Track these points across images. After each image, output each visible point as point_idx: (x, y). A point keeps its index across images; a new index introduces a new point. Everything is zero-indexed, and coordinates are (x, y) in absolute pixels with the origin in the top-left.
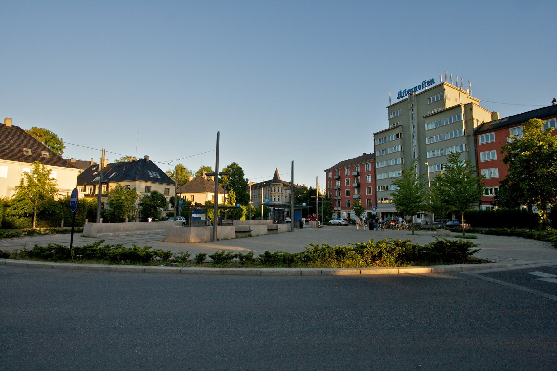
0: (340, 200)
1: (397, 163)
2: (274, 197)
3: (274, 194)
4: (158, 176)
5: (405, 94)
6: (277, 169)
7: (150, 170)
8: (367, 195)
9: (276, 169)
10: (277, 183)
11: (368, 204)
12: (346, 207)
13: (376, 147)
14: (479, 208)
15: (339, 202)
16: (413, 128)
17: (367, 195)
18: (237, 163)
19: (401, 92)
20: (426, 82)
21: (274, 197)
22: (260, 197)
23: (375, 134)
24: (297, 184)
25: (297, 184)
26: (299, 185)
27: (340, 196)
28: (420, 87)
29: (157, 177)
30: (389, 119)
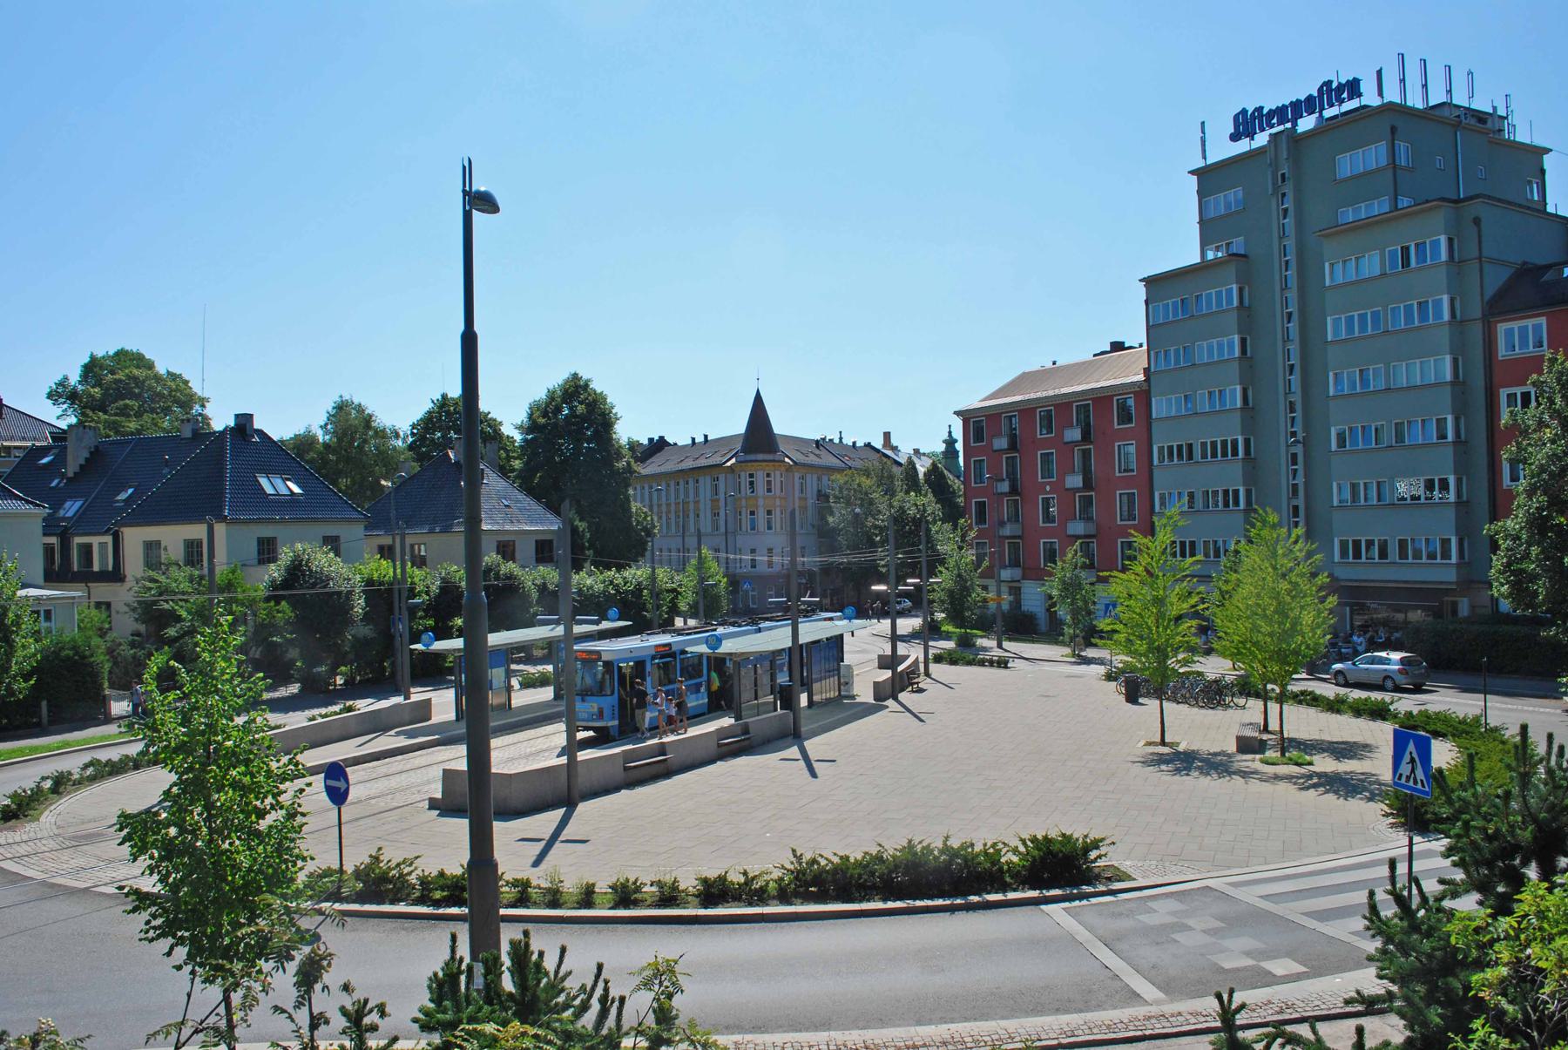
0: (1019, 537)
1: (1228, 407)
5: (1329, 99)
9: (758, 401)
10: (760, 457)
13: (1150, 331)
14: (695, 628)
16: (1286, 270)
17: (1041, 524)
18: (585, 374)
19: (1244, 111)
20: (1265, 112)
23: (1151, 282)
24: (693, 439)
25: (693, 439)
28: (1309, 105)
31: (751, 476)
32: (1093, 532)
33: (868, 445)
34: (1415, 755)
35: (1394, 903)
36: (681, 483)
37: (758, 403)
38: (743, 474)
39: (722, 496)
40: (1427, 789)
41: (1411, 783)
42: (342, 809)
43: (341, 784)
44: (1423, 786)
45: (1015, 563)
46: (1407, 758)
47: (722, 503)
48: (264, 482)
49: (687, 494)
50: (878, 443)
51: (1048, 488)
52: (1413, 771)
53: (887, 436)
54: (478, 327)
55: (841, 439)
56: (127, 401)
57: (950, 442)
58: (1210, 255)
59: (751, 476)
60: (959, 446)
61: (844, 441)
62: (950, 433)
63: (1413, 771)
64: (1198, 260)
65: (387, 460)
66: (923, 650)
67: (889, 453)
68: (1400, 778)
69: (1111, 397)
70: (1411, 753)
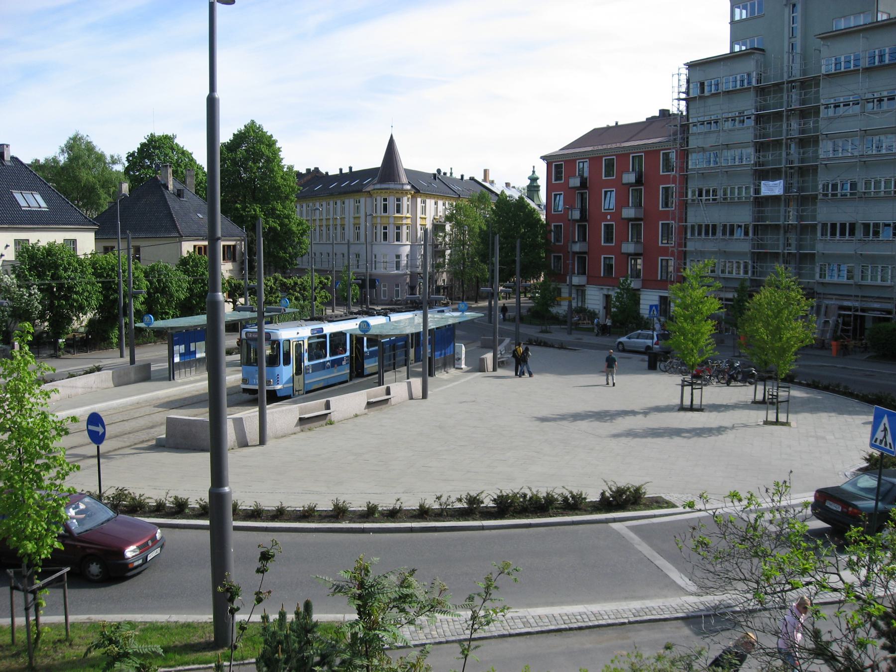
0: (585, 253)
2: (383, 231)
3: (385, 221)
4: (43, 204)
6: (395, 138)
7: (20, 188)
8: (660, 245)
9: (391, 143)
11: (661, 272)
12: (602, 275)
15: (582, 261)
17: (223, 243)
21: (385, 228)
22: (339, 228)
24: (462, 176)
25: (462, 176)
26: (466, 178)
27: (584, 240)
29: (40, 207)
30: (733, 22)
31: (385, 200)
32: (641, 251)
33: (472, 179)
34: (887, 426)
36: (331, 203)
37: (391, 145)
38: (378, 198)
39: (362, 214)
40: (893, 450)
41: (883, 445)
42: (753, 397)
43: (100, 429)
44: (891, 447)
45: (582, 272)
46: (881, 427)
47: (362, 220)
49: (335, 212)
50: (480, 178)
51: (609, 217)
52: (885, 437)
53: (486, 172)
55: (451, 174)
57: (533, 179)
58: (737, 48)
59: (385, 200)
60: (542, 183)
61: (454, 175)
62: (534, 172)
63: (885, 437)
64: (728, 51)
65: (108, 181)
67: (487, 185)
68: (876, 441)
69: (658, 151)
70: (885, 424)
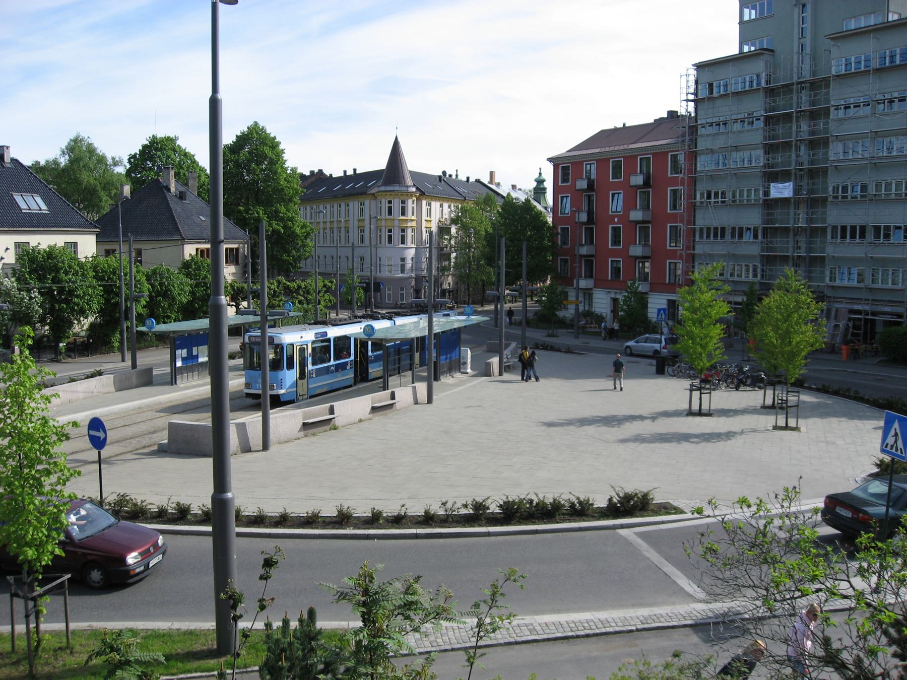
0: (592, 256)
2: (387, 234)
3: (389, 223)
4: (44, 207)
6: (399, 139)
7: (20, 191)
8: (668, 248)
9: (396, 145)
11: (670, 275)
12: (609, 278)
15: (589, 264)
21: (390, 231)
22: (343, 231)
24: (468, 178)
25: (468, 178)
26: (472, 180)
27: (592, 243)
29: (41, 210)
30: (742, 23)
31: (390, 202)
32: (649, 254)
33: (478, 181)
34: (898, 431)
35: (102, 420)
36: (335, 206)
37: (396, 147)
38: (383, 201)
39: (367, 217)
40: (904, 455)
41: (894, 451)
43: (101, 434)
44: (902, 453)
45: (589, 275)
46: (892, 432)
47: (367, 223)
48: (18, 198)
49: (339, 215)
50: (486, 180)
51: (616, 220)
52: (896, 442)
53: (492, 174)
54: (221, 95)
55: (457, 176)
56: (647, 335)
57: (540, 181)
58: (746, 49)
59: (390, 202)
60: (549, 185)
61: (459, 177)
62: (540, 174)
63: (896, 442)
64: (737, 52)
65: (109, 184)
66: (427, 320)
67: (493, 187)
68: (886, 447)
69: (666, 153)
70: (895, 429)
